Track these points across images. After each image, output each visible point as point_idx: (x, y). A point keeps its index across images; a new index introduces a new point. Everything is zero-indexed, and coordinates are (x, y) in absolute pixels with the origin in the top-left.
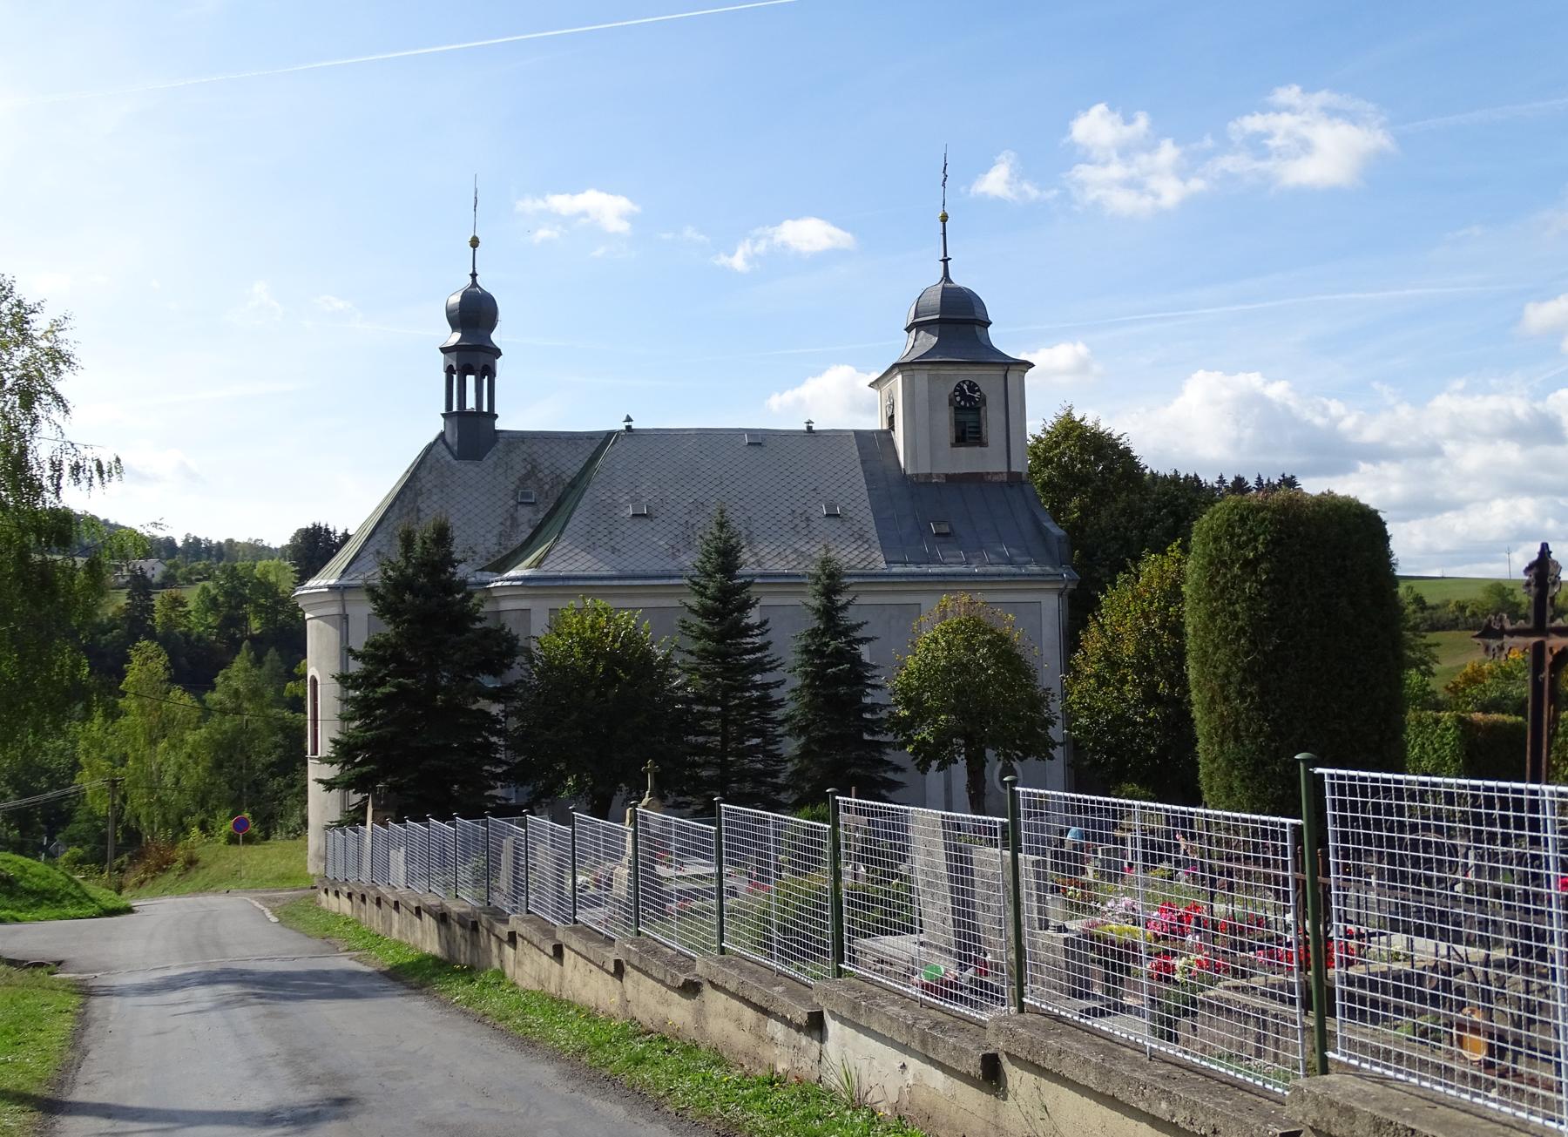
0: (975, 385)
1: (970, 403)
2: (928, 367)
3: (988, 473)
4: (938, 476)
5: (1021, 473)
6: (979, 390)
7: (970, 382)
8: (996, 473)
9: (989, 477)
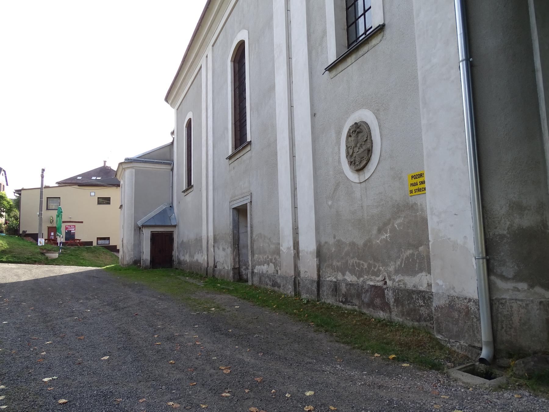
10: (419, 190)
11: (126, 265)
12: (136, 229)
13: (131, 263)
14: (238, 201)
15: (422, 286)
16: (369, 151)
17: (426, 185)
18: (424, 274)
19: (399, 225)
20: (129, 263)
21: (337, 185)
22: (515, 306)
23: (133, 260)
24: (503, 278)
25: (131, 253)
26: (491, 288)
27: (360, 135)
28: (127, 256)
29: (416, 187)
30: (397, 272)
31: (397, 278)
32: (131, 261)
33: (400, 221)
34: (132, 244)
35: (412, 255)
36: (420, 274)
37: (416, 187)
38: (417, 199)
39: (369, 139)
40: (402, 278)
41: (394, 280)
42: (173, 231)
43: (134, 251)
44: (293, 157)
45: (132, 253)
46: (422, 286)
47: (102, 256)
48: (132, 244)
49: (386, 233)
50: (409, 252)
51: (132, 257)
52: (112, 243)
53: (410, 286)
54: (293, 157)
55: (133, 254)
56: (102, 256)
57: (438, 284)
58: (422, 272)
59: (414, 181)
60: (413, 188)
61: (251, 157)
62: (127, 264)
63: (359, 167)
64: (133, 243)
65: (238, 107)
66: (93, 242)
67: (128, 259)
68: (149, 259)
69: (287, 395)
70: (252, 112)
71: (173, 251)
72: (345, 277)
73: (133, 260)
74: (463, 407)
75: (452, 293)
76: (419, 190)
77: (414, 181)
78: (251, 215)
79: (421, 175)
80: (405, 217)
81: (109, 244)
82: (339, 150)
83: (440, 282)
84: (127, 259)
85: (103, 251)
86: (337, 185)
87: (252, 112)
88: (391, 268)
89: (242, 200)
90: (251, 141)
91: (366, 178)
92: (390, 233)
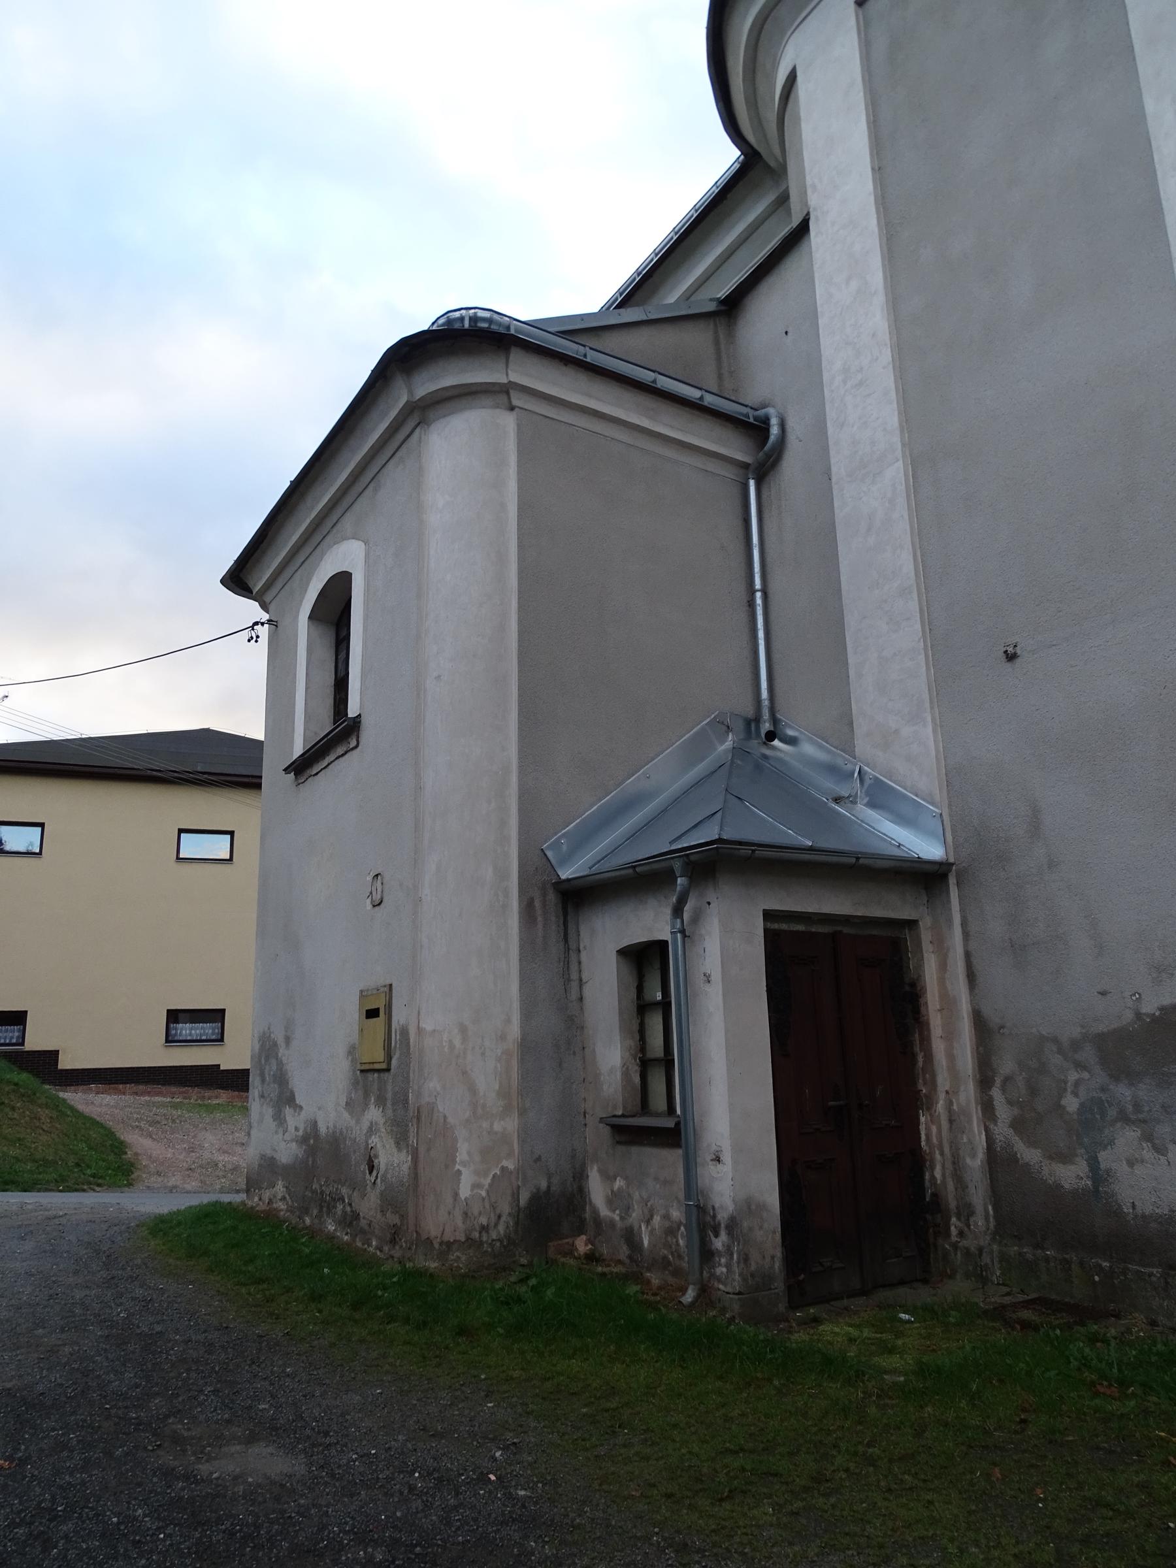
11: (449, 1245)
12: (537, 904)
13: (501, 1228)
20: (484, 1229)
23: (516, 1196)
25: (497, 1127)
28: (462, 1155)
32: (505, 1208)
34: (503, 1037)
42: (912, 924)
43: (522, 1112)
45: (510, 1125)
47: (13, 1109)
48: (503, 1037)
51: (510, 1164)
52: (36, 1040)
55: (522, 1142)
56: (13, 1109)
62: (470, 1242)
64: (515, 1031)
66: (169, 1008)
67: (475, 1186)
68: (773, 1200)
69: (287, 1545)
71: (930, 1107)
72: (984, 1241)
73: (524, 1198)
81: (23, 1044)
84: (465, 1191)
85: (16, 1084)
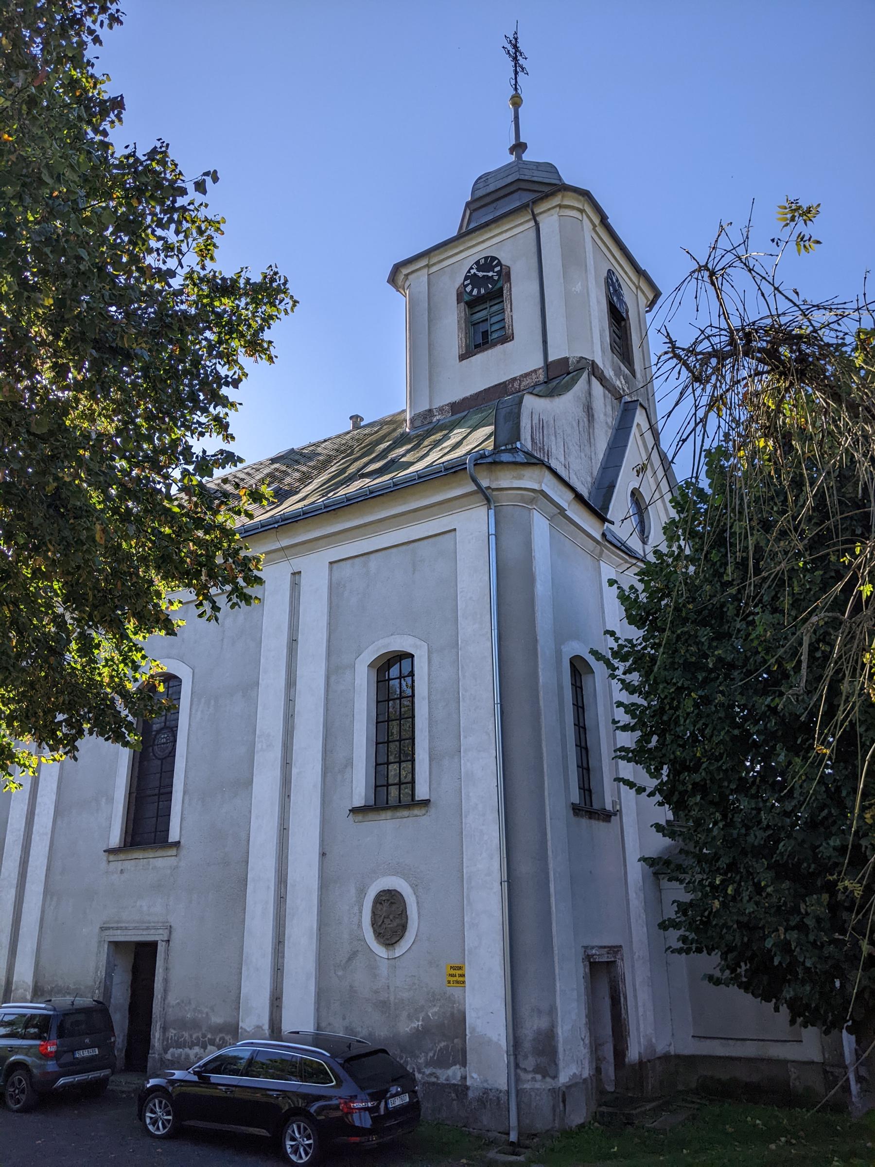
0: (494, 258)
1: (486, 288)
2: (423, 262)
3: (514, 380)
4: (441, 410)
5: (566, 359)
6: (499, 263)
7: (477, 263)
8: (527, 375)
9: (516, 385)
10: (458, 982)
14: (130, 932)
15: (455, 1079)
16: (404, 927)
17: (467, 979)
18: (458, 1066)
19: (434, 1014)
21: (354, 955)
22: (533, 1094)
24: (525, 1070)
26: (518, 1080)
27: (394, 907)
29: (455, 979)
30: (428, 1064)
31: (428, 1071)
33: (436, 1009)
35: (447, 1046)
36: (454, 1067)
37: (455, 979)
38: (456, 991)
39: (403, 915)
40: (434, 1070)
41: (424, 1073)
44: (281, 899)
46: (455, 1079)
49: (418, 1021)
50: (443, 1044)
53: (442, 1080)
54: (281, 899)
57: (473, 1078)
58: (455, 1065)
59: (453, 972)
60: (452, 979)
61: (177, 867)
63: (388, 942)
65: (137, 765)
70: (187, 798)
74: (124, 175)
75: (486, 1085)
76: (458, 982)
77: (453, 972)
78: (166, 960)
79: (460, 968)
80: (440, 1007)
82: (361, 912)
83: (475, 1076)
86: (354, 955)
87: (187, 798)
88: (421, 1060)
89: (140, 932)
90: (179, 842)
91: (397, 955)
92: (423, 1020)
